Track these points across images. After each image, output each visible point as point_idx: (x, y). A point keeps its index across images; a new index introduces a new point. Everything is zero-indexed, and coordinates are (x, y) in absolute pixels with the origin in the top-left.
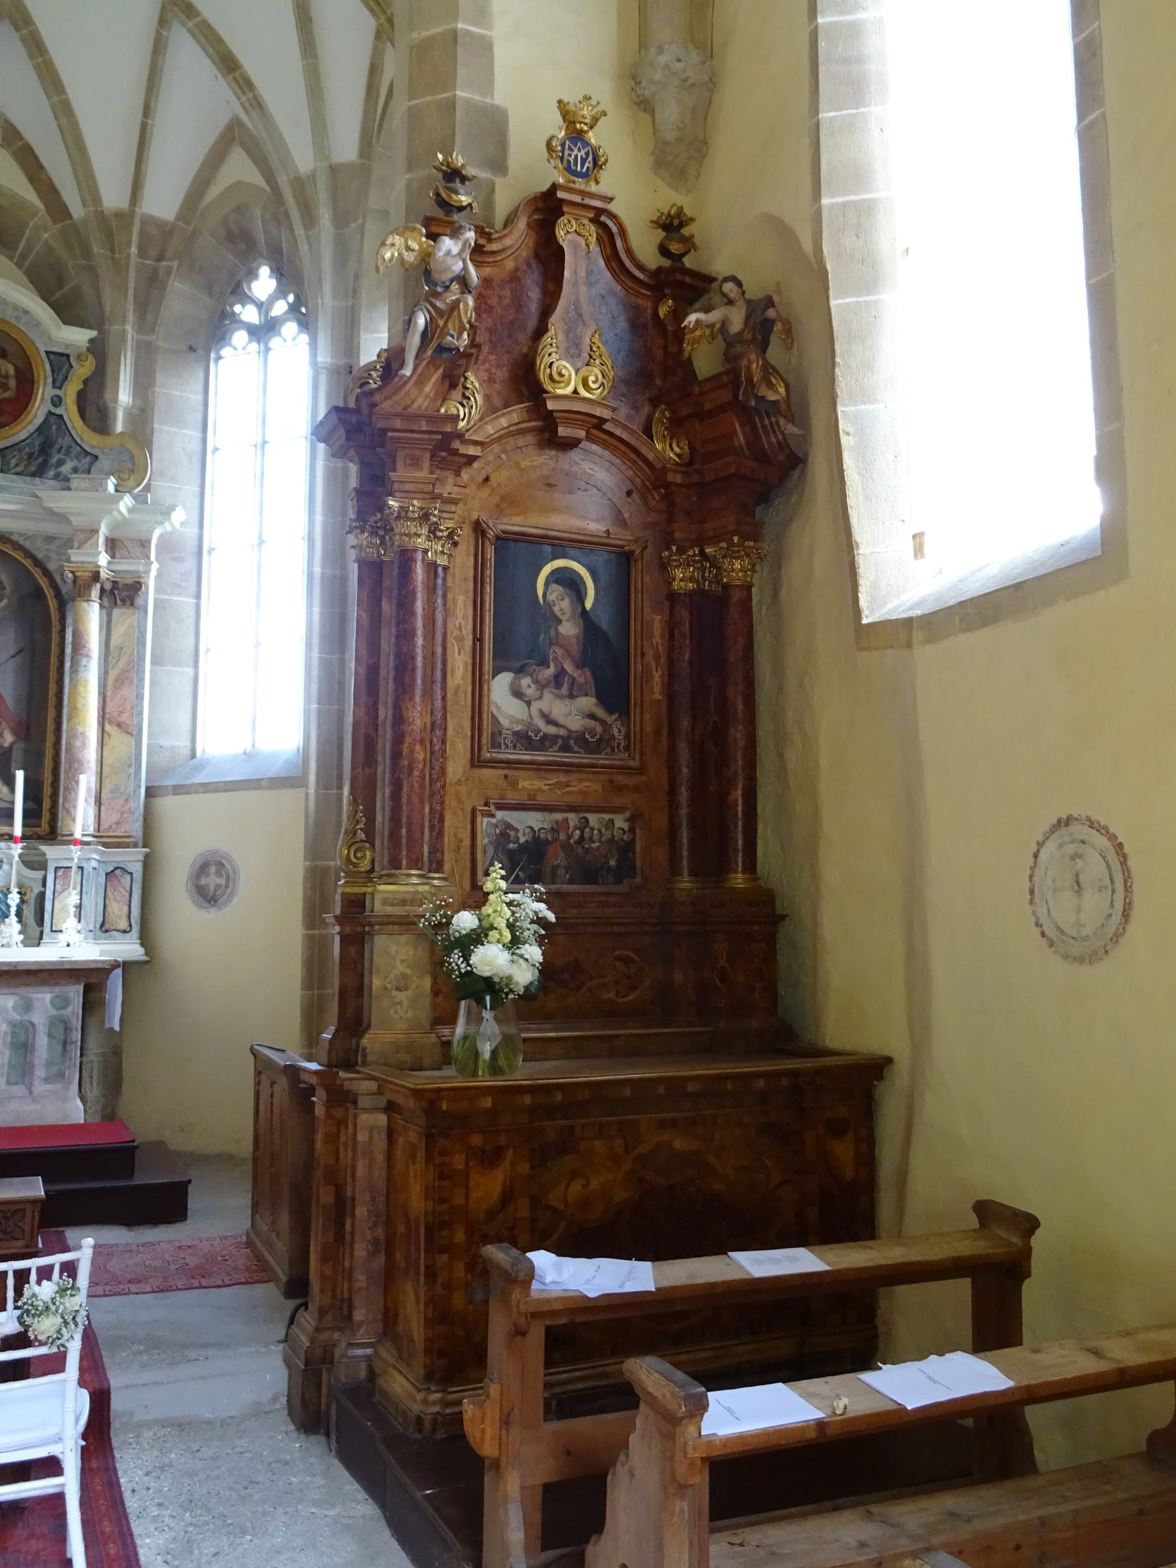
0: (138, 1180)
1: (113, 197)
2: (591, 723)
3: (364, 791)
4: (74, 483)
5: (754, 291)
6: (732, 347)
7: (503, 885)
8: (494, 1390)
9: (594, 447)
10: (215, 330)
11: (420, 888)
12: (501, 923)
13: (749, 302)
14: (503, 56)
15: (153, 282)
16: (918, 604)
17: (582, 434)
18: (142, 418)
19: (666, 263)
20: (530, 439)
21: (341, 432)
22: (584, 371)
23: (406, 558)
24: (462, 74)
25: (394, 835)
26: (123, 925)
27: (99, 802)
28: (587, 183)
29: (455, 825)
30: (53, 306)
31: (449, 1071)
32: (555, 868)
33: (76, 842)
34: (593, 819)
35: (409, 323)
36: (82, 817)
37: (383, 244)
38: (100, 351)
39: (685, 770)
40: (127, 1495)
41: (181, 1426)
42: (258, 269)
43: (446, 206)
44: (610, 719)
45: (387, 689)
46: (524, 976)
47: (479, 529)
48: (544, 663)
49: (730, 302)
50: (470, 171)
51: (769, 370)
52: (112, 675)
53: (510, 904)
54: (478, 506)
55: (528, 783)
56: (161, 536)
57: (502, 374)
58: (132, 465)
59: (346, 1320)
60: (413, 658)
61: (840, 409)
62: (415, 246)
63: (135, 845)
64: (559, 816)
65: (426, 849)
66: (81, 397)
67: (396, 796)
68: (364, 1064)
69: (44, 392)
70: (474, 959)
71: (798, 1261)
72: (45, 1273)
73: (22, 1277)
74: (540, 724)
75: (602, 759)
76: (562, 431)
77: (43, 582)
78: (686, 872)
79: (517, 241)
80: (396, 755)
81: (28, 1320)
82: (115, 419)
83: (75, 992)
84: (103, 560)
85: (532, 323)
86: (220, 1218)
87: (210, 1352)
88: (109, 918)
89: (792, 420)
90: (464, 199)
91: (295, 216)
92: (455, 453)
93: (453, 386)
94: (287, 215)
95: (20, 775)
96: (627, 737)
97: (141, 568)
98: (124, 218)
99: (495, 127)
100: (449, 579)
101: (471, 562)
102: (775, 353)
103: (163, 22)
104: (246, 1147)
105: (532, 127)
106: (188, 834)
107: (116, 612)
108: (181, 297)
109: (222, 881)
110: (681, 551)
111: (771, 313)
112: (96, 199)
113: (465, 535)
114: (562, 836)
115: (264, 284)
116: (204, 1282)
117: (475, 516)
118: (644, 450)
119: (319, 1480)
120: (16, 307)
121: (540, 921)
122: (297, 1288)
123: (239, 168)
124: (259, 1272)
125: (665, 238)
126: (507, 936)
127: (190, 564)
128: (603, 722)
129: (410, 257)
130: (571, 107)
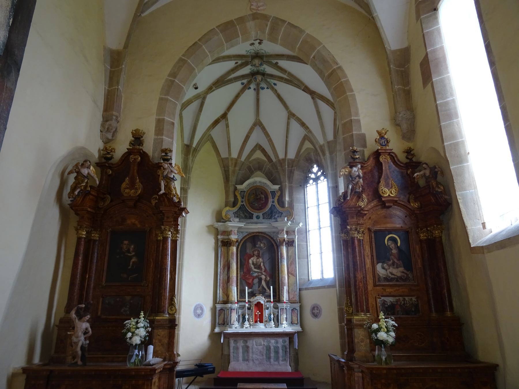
0: (305, 387)
1: (281, 156)
2: (403, 274)
3: (348, 294)
4: (278, 220)
5: (431, 166)
6: (427, 179)
7: (384, 317)
10: (305, 181)
13: (430, 168)
14: (362, 122)
15: (291, 172)
16: (485, 242)
17: (392, 204)
19: (408, 161)
20: (380, 207)
21: (335, 212)
22: (390, 190)
23: (353, 239)
24: (354, 128)
26: (296, 322)
29: (371, 301)
30: (270, 181)
32: (398, 311)
33: (284, 303)
34: (407, 298)
35: (348, 187)
36: (285, 297)
38: (281, 190)
39: (430, 285)
44: (408, 273)
46: (391, 340)
47: (369, 230)
49: (425, 169)
50: (358, 150)
51: (438, 184)
52: (289, 263)
53: (386, 322)
54: (369, 224)
55: (388, 290)
57: (370, 193)
58: (290, 215)
60: (357, 262)
61: (457, 193)
64: (397, 298)
65: (365, 308)
68: (355, 361)
69: (270, 200)
70: (378, 336)
74: (390, 275)
75: (407, 283)
76: (387, 204)
77: (273, 242)
78: (434, 311)
79: (371, 163)
80: (355, 285)
83: (287, 339)
84: (285, 236)
85: (377, 181)
88: (293, 320)
90: (357, 156)
91: (321, 154)
92: (362, 213)
93: (360, 198)
94: (319, 154)
95: (272, 287)
96: (413, 277)
98: (284, 160)
99: (363, 139)
102: (439, 178)
103: (289, 119)
104: (329, 380)
105: (371, 136)
107: (289, 248)
108: (297, 175)
110: (421, 229)
111: (436, 170)
112: (278, 157)
113: (366, 231)
114: (399, 303)
115: (315, 169)
117: (368, 227)
118: (408, 206)
120: (263, 183)
121: (394, 326)
123: (308, 145)
125: (407, 155)
126: (386, 330)
127: (304, 235)
128: (406, 274)
129: (346, 173)
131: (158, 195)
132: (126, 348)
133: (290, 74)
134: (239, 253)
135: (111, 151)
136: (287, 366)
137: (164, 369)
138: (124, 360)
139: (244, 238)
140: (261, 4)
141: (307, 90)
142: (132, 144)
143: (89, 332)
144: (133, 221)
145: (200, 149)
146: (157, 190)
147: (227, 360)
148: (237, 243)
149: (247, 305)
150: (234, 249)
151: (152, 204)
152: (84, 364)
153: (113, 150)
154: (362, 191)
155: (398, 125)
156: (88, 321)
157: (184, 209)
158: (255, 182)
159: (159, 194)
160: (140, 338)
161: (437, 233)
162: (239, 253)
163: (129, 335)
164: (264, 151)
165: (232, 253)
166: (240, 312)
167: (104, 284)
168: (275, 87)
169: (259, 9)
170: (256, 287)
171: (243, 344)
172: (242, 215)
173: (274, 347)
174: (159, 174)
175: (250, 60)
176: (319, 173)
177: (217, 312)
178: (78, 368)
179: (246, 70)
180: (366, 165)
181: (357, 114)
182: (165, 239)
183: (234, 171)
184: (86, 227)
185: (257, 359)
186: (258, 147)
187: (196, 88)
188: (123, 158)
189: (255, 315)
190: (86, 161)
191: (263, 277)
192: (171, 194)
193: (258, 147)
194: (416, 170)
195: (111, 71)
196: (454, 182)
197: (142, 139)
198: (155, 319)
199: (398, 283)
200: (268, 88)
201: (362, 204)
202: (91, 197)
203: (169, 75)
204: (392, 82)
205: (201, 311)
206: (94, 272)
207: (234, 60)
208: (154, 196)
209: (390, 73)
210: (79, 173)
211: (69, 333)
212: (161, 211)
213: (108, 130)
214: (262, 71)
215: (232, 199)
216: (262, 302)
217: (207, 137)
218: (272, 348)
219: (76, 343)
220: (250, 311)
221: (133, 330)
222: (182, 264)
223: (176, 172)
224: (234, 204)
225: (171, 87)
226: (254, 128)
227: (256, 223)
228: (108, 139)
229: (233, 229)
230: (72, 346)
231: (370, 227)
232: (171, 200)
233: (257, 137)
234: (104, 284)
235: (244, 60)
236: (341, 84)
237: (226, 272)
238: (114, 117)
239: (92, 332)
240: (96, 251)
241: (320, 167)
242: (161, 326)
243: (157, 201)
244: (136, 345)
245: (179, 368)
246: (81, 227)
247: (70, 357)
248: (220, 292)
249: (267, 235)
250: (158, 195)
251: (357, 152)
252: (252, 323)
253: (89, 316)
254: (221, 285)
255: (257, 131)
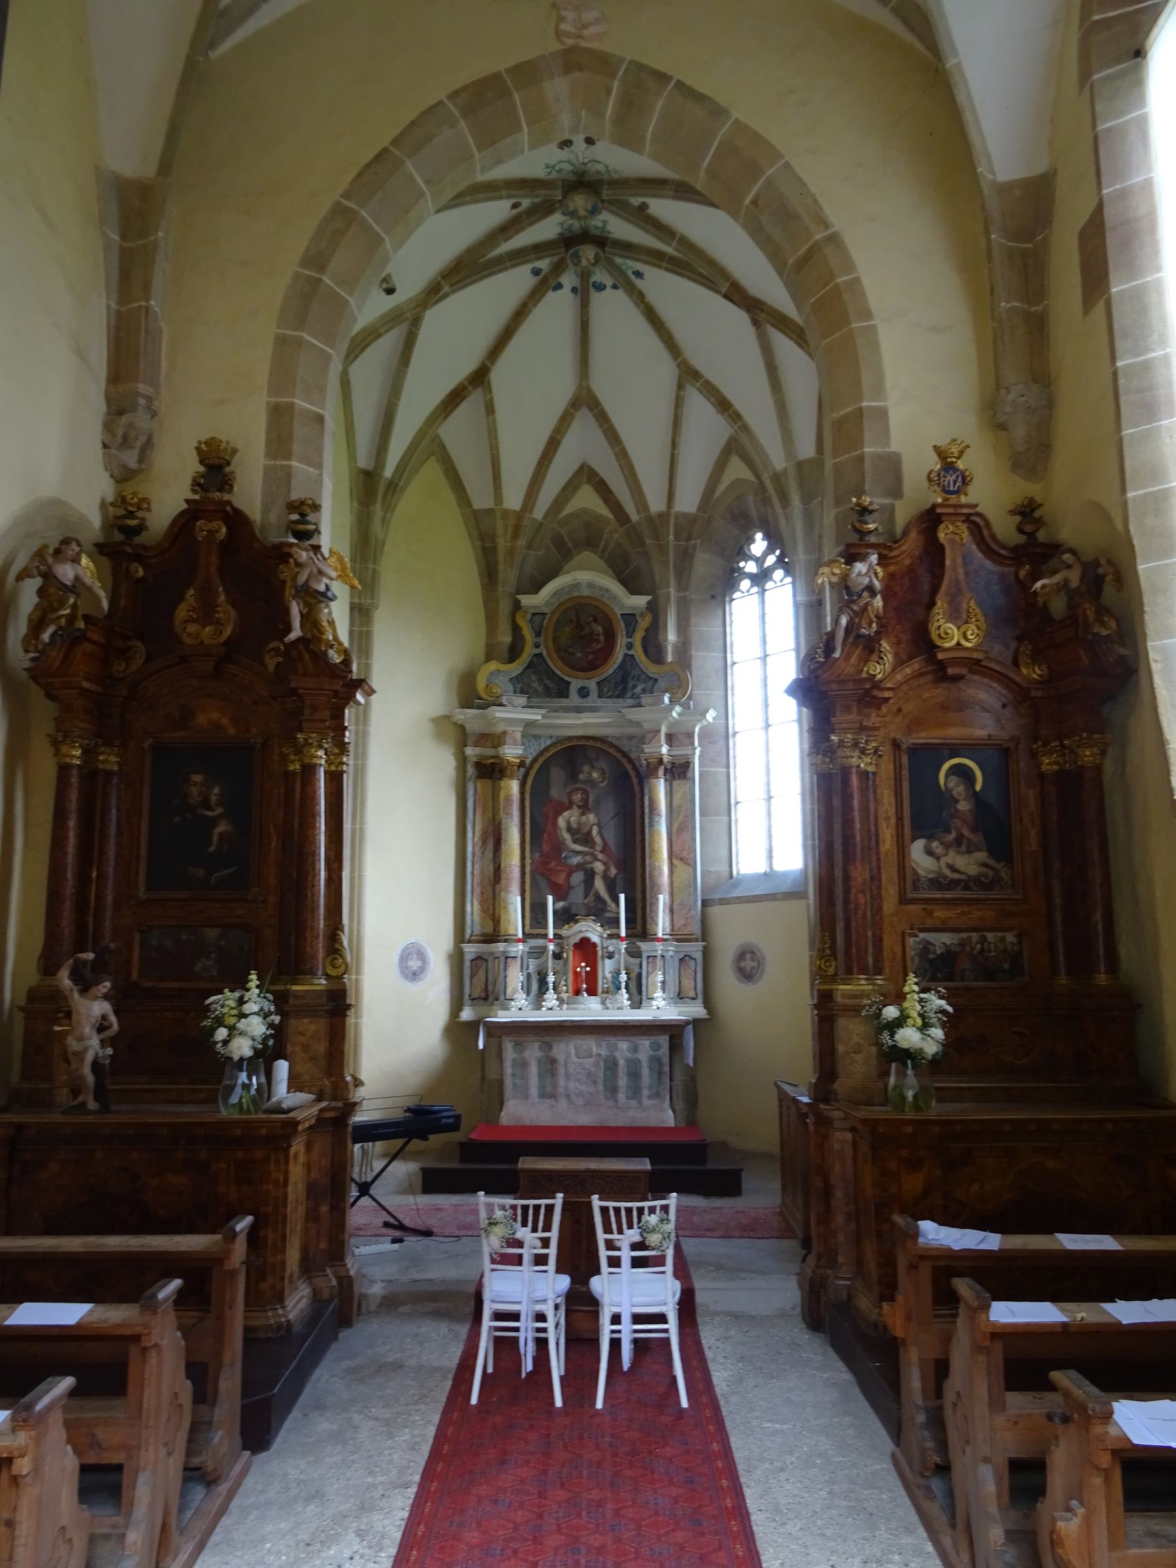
0: (710, 1166)
1: (656, 504)
2: (984, 870)
7: (916, 988)
8: (900, 1298)
9: (976, 677)
10: (728, 581)
11: (867, 987)
12: (914, 1014)
13: (1083, 564)
15: (685, 558)
17: (964, 671)
18: (684, 649)
19: (1022, 539)
20: (929, 677)
22: (963, 628)
24: (867, 436)
25: (848, 953)
26: (692, 994)
27: (672, 911)
28: (959, 497)
31: (888, 1108)
33: (659, 940)
34: (990, 936)
36: (662, 924)
37: (816, 574)
38: (655, 609)
39: (1058, 900)
40: (706, 1350)
41: (737, 1317)
42: (754, 535)
43: (862, 534)
44: (999, 866)
45: (839, 857)
46: (931, 1049)
47: (896, 745)
48: (948, 831)
51: (1103, 611)
53: (921, 1000)
55: (940, 913)
56: (701, 729)
57: (905, 637)
58: (679, 686)
59: (833, 1263)
60: (854, 837)
62: (837, 571)
63: (697, 940)
64: (965, 935)
65: (870, 960)
66: (645, 642)
67: (847, 928)
68: (836, 1100)
69: (621, 641)
70: (897, 1037)
71: (1106, 1243)
72: (652, 1210)
73: (641, 1211)
74: (948, 872)
75: (993, 895)
76: (950, 671)
77: (628, 767)
79: (912, 545)
80: (846, 901)
81: (645, 1235)
82: (666, 652)
83: (664, 1040)
84: (665, 750)
86: (762, 1195)
87: (753, 1275)
89: (1124, 645)
90: (871, 526)
92: (875, 697)
93: (872, 651)
94: (769, 499)
95: (622, 897)
97: (689, 752)
98: (664, 517)
99: (892, 466)
100: (878, 780)
101: (891, 766)
102: (1109, 593)
103: (680, 386)
104: (776, 1150)
105: (918, 465)
106: (733, 931)
107: (675, 783)
108: (704, 563)
109: (754, 964)
110: (1046, 744)
111: (1100, 571)
113: (886, 750)
115: (759, 545)
116: (751, 1234)
117: (892, 735)
118: (1012, 675)
119: (820, 1357)
120: (601, 588)
121: (943, 1012)
122: (806, 1244)
123: (737, 470)
124: (786, 1232)
125: (1021, 522)
126: (919, 1022)
127: (721, 745)
129: (835, 579)
130: (943, 448)
131: (284, 644)
132: (219, 1067)
133: (685, 243)
134: (527, 797)
135: (139, 508)
136: (662, 1110)
137: (320, 1120)
138: (211, 1099)
139: (541, 753)
140: (588, 16)
141: (737, 295)
142: (199, 485)
143: (110, 1027)
144: (215, 716)
145: (407, 483)
146: (281, 627)
147: (494, 1094)
148: (522, 770)
149: (551, 947)
150: (514, 786)
151: (265, 666)
152: (105, 1109)
153: (144, 504)
154: (877, 633)
155: (1002, 427)
156: (106, 997)
157: (360, 683)
158: (576, 586)
159: (286, 640)
160: (251, 1043)
161: (1087, 755)
162: (527, 797)
163: (222, 1033)
164: (602, 488)
165: (508, 799)
166: (533, 965)
167: (142, 893)
168: (638, 283)
169: (585, 32)
170: (577, 896)
171: (539, 1054)
172: (536, 685)
173: (628, 1061)
174: (283, 576)
175: (558, 194)
176: (771, 560)
177: (467, 964)
178: (90, 1118)
179: (548, 228)
180: (895, 553)
181: (879, 391)
182: (309, 771)
183: (511, 552)
184: (79, 737)
185: (581, 1094)
186: (587, 475)
187: (390, 291)
188: (176, 530)
189: (576, 973)
190: (66, 541)
191: (599, 867)
192: (320, 640)
193: (587, 475)
194: (1044, 568)
195: (123, 252)
196: (1143, 612)
197: (228, 469)
198: (288, 991)
199: (968, 895)
200: (615, 287)
201: (877, 670)
202: (89, 647)
203: (306, 261)
204: (992, 289)
205: (419, 963)
206: (112, 862)
207: (509, 197)
208: (272, 645)
209: (990, 260)
210: (48, 576)
211: (57, 1028)
212: (294, 691)
213: (125, 443)
214: (597, 233)
215: (506, 638)
216: (595, 939)
217: (429, 445)
218: (622, 1062)
219: (80, 1056)
220: (561, 962)
221: (232, 1021)
222: (362, 830)
223: (334, 574)
224: (513, 654)
225: (310, 301)
226: (573, 416)
227: (579, 710)
228: (125, 467)
229: (510, 729)
230: (68, 1062)
231: (898, 737)
232: (320, 658)
233: (582, 445)
234: (142, 893)
235: (539, 196)
236: (837, 292)
237: (489, 854)
238: (142, 401)
239: (120, 1024)
240: (114, 802)
241: (774, 539)
242: (308, 1009)
243: (281, 659)
244: (242, 1059)
245: (359, 1118)
246: (65, 737)
247: (65, 1091)
248: (473, 908)
249: (612, 745)
250: (284, 644)
251: (871, 512)
252: (564, 996)
253: (108, 984)
254: (478, 890)
255: (583, 423)
